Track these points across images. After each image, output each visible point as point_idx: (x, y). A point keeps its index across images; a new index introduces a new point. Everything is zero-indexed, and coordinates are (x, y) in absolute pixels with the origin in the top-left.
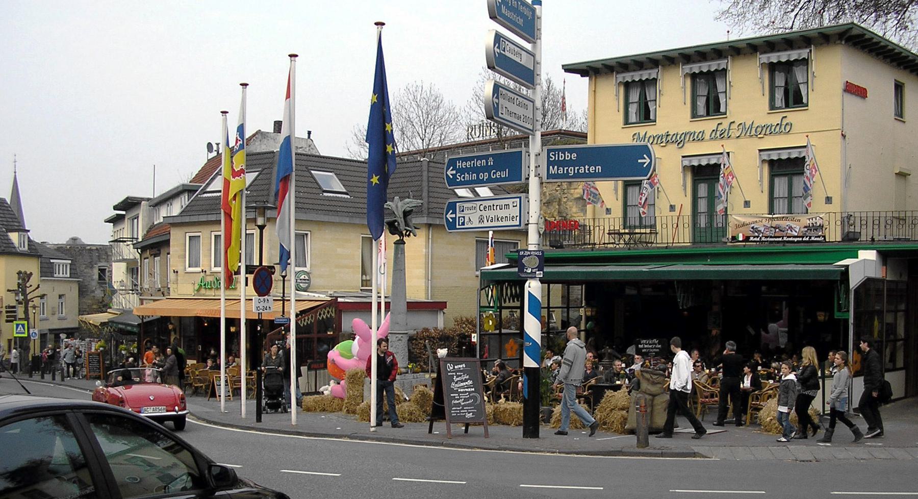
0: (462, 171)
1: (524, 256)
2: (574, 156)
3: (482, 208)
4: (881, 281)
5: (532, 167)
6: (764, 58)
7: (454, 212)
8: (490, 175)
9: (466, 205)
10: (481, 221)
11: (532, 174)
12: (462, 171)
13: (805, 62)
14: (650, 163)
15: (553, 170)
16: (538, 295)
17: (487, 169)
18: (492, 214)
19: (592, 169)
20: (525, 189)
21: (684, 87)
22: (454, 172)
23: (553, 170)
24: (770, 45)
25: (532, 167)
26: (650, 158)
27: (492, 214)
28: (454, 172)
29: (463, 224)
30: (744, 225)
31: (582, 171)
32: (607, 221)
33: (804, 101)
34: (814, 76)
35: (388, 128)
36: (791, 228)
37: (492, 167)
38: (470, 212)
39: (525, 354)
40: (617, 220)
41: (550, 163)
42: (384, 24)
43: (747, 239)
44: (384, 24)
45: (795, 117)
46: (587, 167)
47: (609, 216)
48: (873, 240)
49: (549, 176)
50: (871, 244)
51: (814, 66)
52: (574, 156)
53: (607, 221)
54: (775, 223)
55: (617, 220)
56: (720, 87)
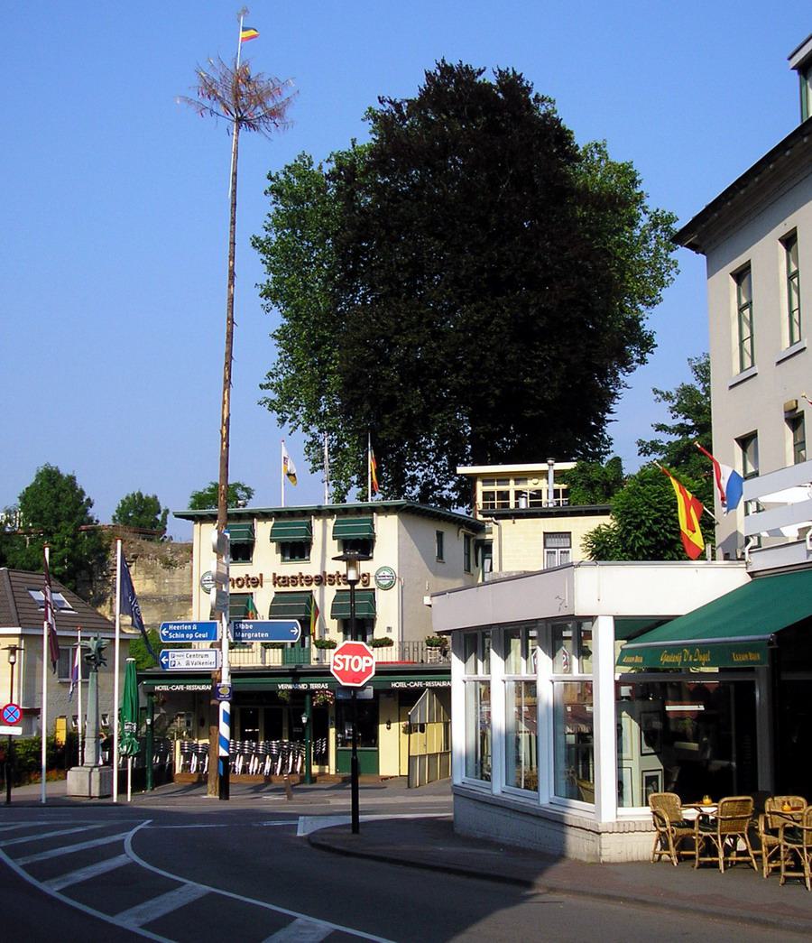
2: (251, 627)
7: (167, 657)
9: (176, 653)
10: (188, 664)
17: (189, 632)
18: (196, 660)
19: (262, 635)
27: (196, 660)
31: (256, 636)
37: (195, 631)
52: (251, 627)
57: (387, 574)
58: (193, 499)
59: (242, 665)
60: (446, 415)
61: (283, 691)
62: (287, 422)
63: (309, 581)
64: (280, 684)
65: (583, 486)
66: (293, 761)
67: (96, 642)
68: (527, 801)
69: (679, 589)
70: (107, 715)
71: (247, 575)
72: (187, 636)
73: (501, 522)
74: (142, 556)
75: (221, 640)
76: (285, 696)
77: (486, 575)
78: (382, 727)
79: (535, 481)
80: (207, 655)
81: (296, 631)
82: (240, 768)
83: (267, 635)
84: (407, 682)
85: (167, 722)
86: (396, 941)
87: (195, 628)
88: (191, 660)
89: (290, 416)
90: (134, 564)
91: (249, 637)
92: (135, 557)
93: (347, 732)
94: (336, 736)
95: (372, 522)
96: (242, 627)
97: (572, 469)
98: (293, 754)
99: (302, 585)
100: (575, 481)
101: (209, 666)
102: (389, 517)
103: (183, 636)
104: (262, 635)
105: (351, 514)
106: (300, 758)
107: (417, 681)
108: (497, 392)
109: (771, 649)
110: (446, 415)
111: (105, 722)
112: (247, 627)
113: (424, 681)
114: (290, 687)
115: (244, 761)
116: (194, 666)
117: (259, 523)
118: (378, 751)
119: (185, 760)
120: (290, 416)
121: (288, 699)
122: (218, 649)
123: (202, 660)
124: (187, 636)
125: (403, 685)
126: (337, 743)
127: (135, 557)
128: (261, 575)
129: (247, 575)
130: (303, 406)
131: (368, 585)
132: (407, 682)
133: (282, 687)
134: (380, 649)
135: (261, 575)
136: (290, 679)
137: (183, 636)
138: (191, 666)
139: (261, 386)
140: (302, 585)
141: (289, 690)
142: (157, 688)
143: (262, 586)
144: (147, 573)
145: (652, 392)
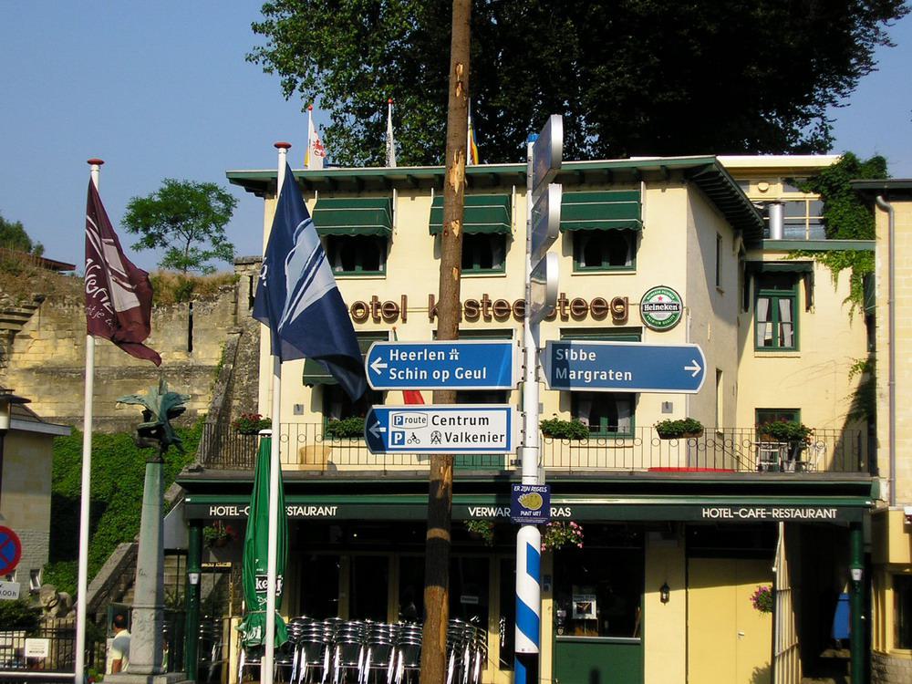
0: (400, 365)
1: (521, 493)
2: (592, 356)
3: (437, 420)
4: (446, 541)
8: (452, 374)
10: (436, 438)
14: (701, 373)
16: (536, 545)
17: (450, 365)
18: (456, 430)
19: (618, 376)
22: (385, 366)
26: (701, 364)
27: (456, 430)
28: (385, 366)
29: (401, 442)
32: (293, 428)
38: (413, 425)
39: (518, 631)
40: (311, 428)
42: (289, 146)
44: (289, 146)
46: (611, 372)
52: (592, 356)
53: (293, 428)
55: (311, 428)
57: (666, 299)
58: (130, 211)
59: (388, 468)
60: (610, 68)
61: (478, 520)
62: (296, 91)
63: (502, 310)
64: (473, 505)
65: (852, 197)
66: (471, 660)
67: (161, 397)
69: (353, 458)
70: (37, 571)
71: (375, 298)
73: (894, 205)
74: (52, 299)
76: (484, 530)
77: (760, 326)
78: (651, 599)
79: (763, 186)
80: (485, 421)
81: (698, 369)
82: (367, 673)
83: (628, 375)
84: (735, 507)
85: (123, 586)
88: (447, 429)
89: (300, 81)
90: (37, 312)
92: (39, 300)
93: (575, 606)
94: (554, 614)
95: (637, 196)
96: (572, 355)
97: (833, 167)
98: (471, 647)
99: (488, 319)
100: (839, 187)
101: (492, 444)
102: (669, 191)
104: (618, 376)
105: (591, 185)
106: (478, 654)
107: (754, 506)
108: (712, 28)
110: (610, 68)
111: (35, 584)
112: (583, 356)
113: (769, 507)
114: (492, 512)
115: (376, 659)
116: (452, 444)
117: (400, 198)
118: (640, 645)
119: (248, 659)
120: (300, 81)
121: (489, 537)
123: (479, 430)
124: (436, 374)
125: (724, 513)
126: (555, 627)
127: (39, 300)
128: (404, 298)
129: (375, 298)
130: (314, 63)
131: (625, 321)
132: (735, 507)
133: (476, 512)
134: (674, 441)
135: (404, 298)
136: (491, 499)
138: (444, 444)
139: (255, 28)
140: (488, 319)
141: (488, 519)
142: (215, 511)
143: (404, 320)
144: (60, 328)
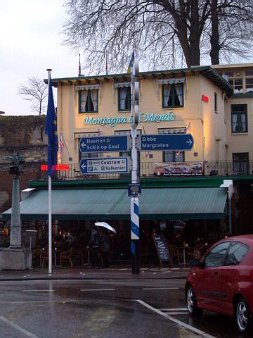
0: (90, 145)
5: (134, 144)
6: (161, 82)
9: (93, 161)
10: (103, 168)
11: (134, 147)
12: (90, 145)
13: (182, 85)
15: (144, 146)
17: (104, 144)
18: (109, 166)
20: (130, 154)
21: (75, 96)
23: (144, 146)
24: (163, 75)
25: (134, 144)
27: (109, 166)
29: (92, 170)
30: (161, 167)
31: (159, 146)
33: (181, 104)
34: (187, 92)
35: (55, 123)
36: (185, 169)
37: (109, 143)
41: (142, 142)
43: (162, 174)
45: (177, 112)
47: (71, 162)
48: (227, 174)
49: (142, 148)
50: (227, 177)
51: (187, 88)
54: (178, 166)
56: (94, 97)
68: (6, 278)
72: (102, 147)
75: (131, 150)
80: (119, 162)
86: (215, 336)
87: (108, 141)
88: (105, 166)
91: (154, 147)
103: (98, 147)
109: (57, 262)
122: (128, 157)
124: (102, 147)
137: (98, 147)
145: (201, 98)
